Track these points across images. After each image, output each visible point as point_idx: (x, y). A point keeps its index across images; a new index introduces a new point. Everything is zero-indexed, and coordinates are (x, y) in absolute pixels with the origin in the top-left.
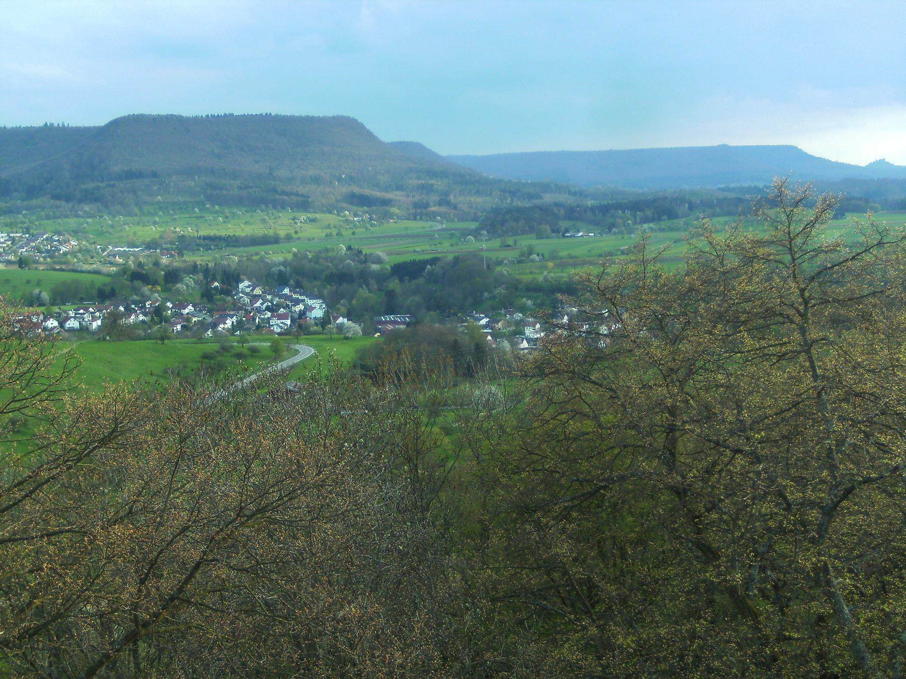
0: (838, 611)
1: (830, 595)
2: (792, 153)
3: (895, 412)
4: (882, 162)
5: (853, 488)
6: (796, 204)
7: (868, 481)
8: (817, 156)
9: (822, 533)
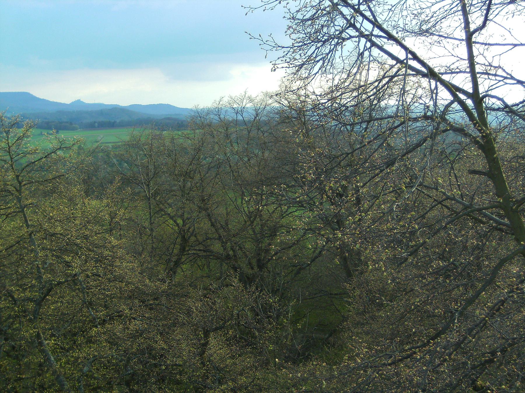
0: (49, 359)
1: (43, 351)
2: (27, 97)
3: (74, 243)
4: (79, 101)
5: (52, 288)
6: (12, 126)
7: (59, 283)
8: (42, 98)
9: (36, 316)
